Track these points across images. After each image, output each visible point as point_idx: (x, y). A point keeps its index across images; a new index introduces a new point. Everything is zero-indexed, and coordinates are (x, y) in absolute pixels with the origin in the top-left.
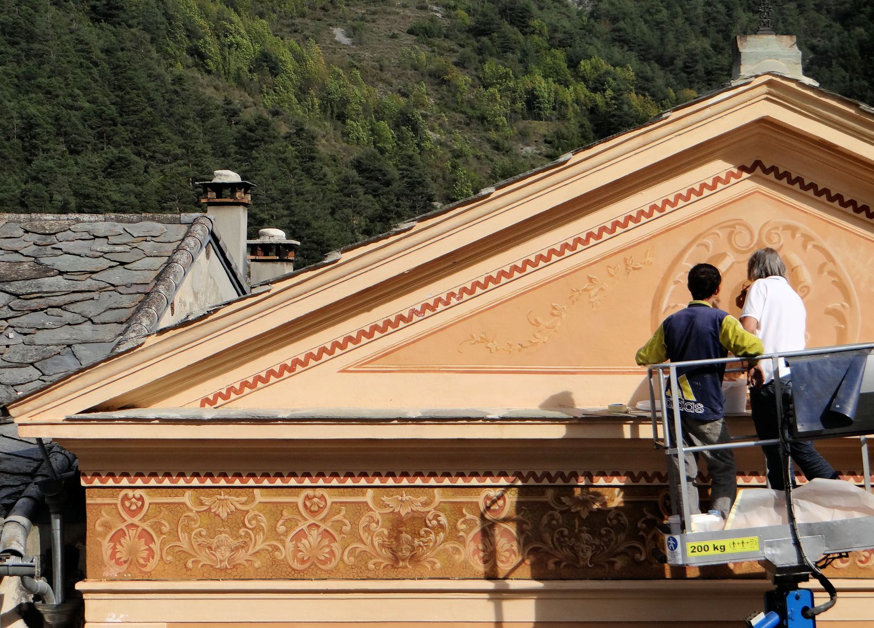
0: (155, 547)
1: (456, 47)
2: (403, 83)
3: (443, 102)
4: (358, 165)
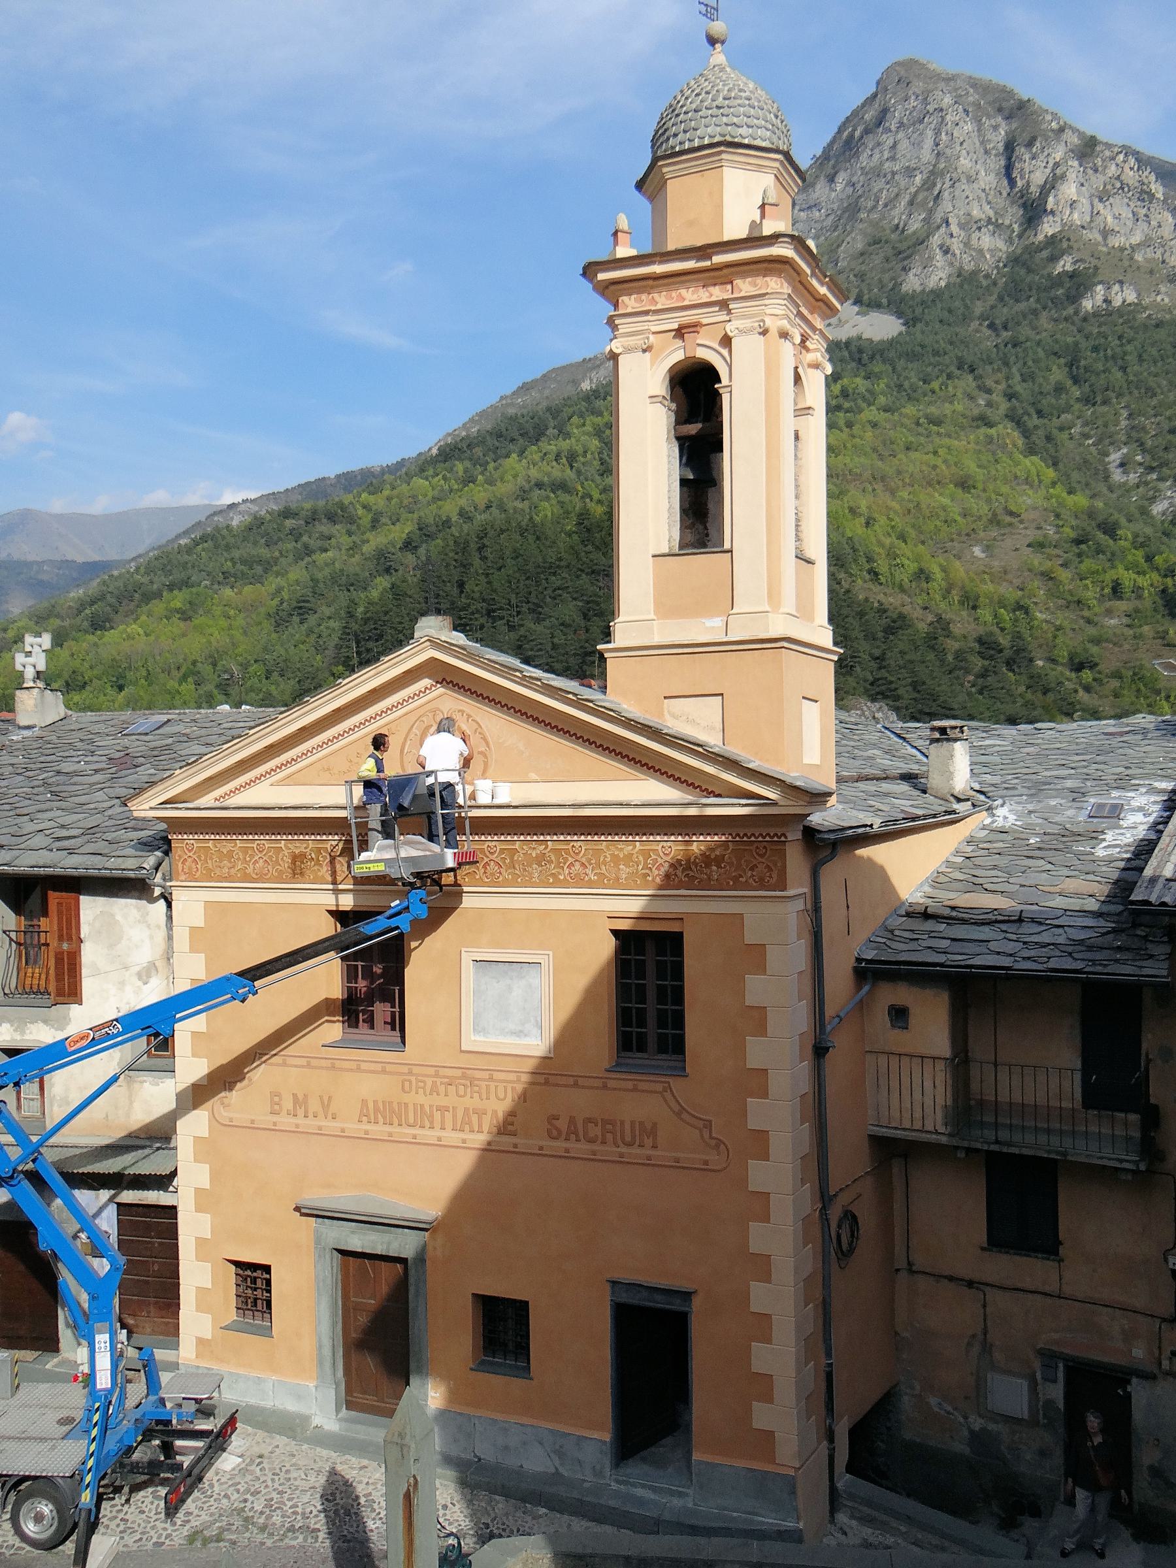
0: (199, 866)
1: (1062, 554)
4: (980, 641)
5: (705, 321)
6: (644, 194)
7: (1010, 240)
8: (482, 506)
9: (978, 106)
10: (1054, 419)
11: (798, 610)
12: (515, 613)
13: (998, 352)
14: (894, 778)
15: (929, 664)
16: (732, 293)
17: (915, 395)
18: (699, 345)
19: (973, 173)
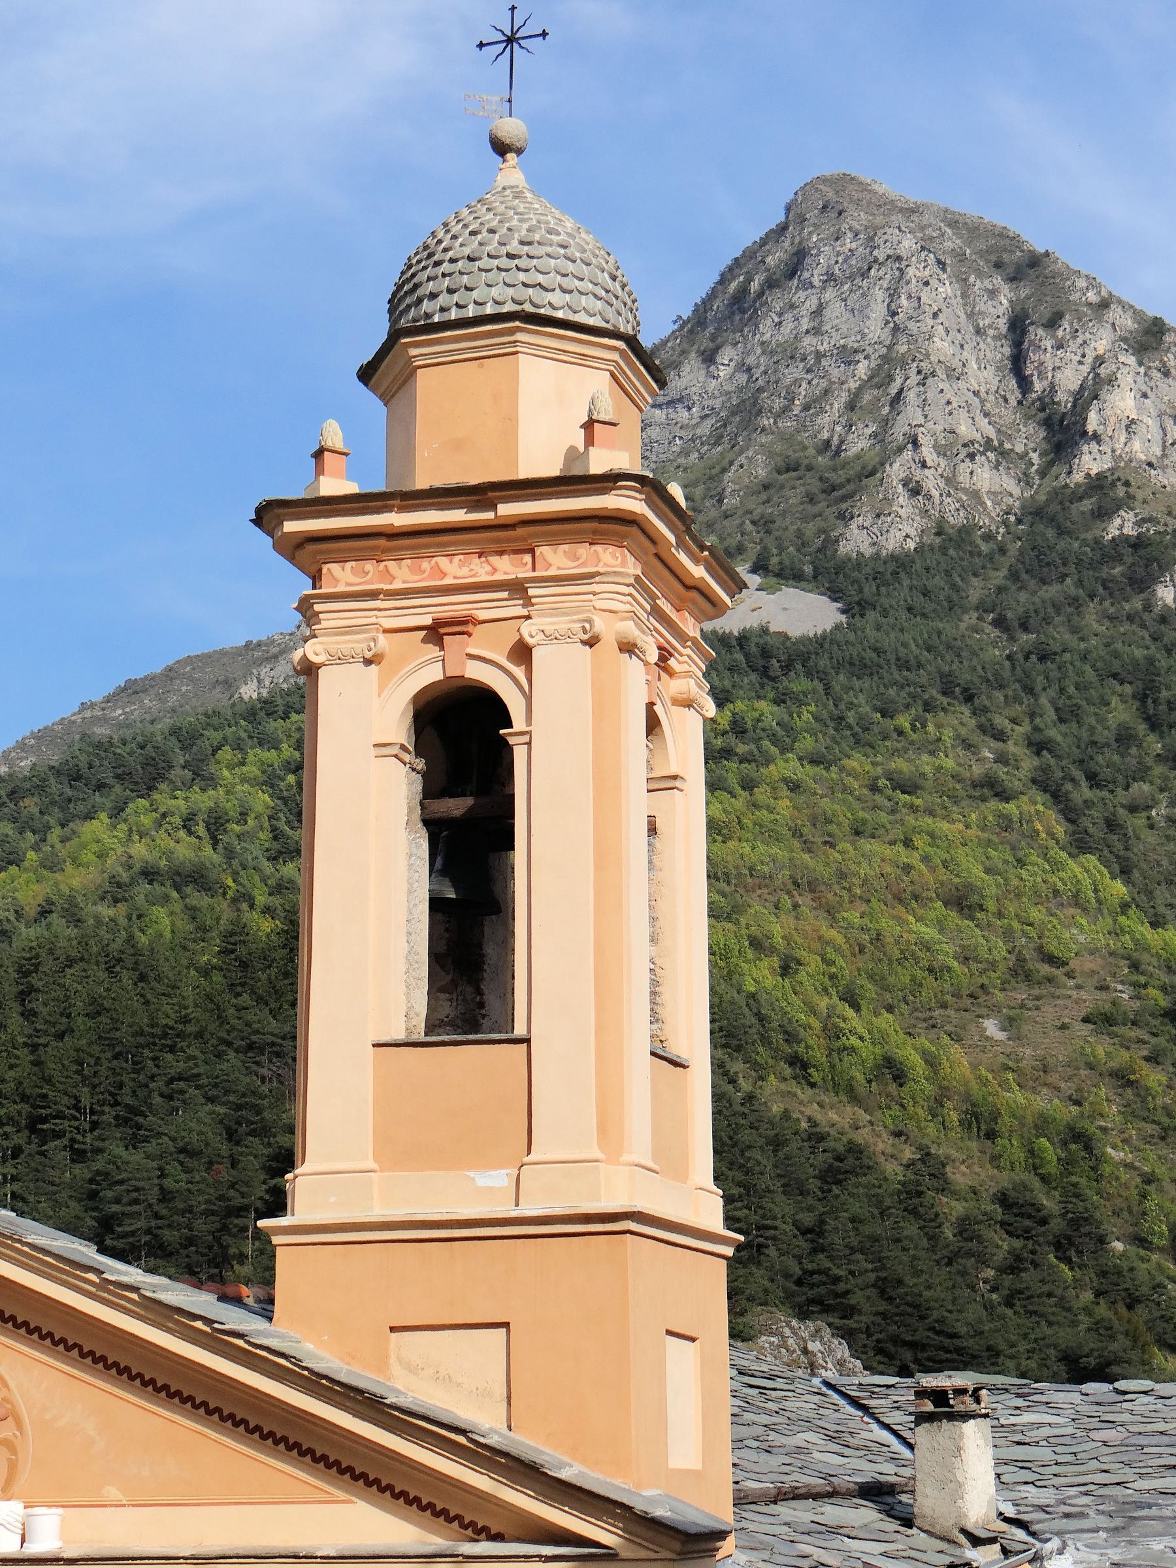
1: (1146, 1037)
2: (1074, 1086)
3: (1129, 1110)
4: (1003, 1199)
5: (482, 615)
6: (374, 390)
7: (1025, 480)
8: (31, 911)
9: (961, 257)
10: (1120, 791)
11: (655, 1158)
12: (87, 1126)
13: (1013, 667)
14: (848, 1494)
15: (906, 1243)
16: (534, 569)
17: (867, 736)
18: (471, 657)
19: (956, 363)
